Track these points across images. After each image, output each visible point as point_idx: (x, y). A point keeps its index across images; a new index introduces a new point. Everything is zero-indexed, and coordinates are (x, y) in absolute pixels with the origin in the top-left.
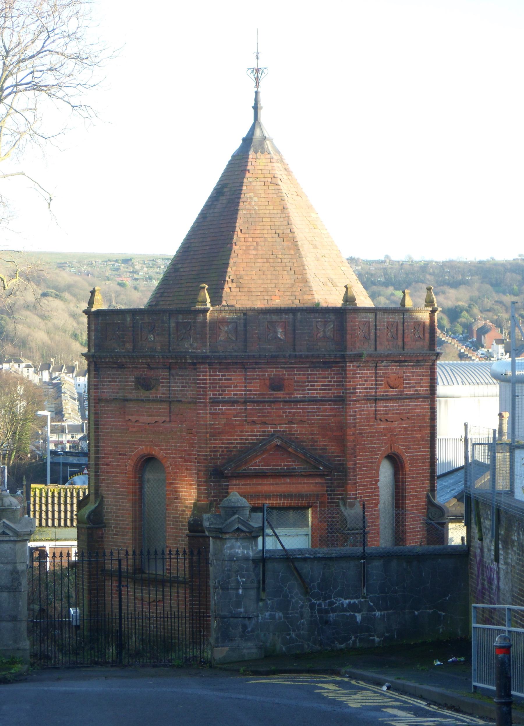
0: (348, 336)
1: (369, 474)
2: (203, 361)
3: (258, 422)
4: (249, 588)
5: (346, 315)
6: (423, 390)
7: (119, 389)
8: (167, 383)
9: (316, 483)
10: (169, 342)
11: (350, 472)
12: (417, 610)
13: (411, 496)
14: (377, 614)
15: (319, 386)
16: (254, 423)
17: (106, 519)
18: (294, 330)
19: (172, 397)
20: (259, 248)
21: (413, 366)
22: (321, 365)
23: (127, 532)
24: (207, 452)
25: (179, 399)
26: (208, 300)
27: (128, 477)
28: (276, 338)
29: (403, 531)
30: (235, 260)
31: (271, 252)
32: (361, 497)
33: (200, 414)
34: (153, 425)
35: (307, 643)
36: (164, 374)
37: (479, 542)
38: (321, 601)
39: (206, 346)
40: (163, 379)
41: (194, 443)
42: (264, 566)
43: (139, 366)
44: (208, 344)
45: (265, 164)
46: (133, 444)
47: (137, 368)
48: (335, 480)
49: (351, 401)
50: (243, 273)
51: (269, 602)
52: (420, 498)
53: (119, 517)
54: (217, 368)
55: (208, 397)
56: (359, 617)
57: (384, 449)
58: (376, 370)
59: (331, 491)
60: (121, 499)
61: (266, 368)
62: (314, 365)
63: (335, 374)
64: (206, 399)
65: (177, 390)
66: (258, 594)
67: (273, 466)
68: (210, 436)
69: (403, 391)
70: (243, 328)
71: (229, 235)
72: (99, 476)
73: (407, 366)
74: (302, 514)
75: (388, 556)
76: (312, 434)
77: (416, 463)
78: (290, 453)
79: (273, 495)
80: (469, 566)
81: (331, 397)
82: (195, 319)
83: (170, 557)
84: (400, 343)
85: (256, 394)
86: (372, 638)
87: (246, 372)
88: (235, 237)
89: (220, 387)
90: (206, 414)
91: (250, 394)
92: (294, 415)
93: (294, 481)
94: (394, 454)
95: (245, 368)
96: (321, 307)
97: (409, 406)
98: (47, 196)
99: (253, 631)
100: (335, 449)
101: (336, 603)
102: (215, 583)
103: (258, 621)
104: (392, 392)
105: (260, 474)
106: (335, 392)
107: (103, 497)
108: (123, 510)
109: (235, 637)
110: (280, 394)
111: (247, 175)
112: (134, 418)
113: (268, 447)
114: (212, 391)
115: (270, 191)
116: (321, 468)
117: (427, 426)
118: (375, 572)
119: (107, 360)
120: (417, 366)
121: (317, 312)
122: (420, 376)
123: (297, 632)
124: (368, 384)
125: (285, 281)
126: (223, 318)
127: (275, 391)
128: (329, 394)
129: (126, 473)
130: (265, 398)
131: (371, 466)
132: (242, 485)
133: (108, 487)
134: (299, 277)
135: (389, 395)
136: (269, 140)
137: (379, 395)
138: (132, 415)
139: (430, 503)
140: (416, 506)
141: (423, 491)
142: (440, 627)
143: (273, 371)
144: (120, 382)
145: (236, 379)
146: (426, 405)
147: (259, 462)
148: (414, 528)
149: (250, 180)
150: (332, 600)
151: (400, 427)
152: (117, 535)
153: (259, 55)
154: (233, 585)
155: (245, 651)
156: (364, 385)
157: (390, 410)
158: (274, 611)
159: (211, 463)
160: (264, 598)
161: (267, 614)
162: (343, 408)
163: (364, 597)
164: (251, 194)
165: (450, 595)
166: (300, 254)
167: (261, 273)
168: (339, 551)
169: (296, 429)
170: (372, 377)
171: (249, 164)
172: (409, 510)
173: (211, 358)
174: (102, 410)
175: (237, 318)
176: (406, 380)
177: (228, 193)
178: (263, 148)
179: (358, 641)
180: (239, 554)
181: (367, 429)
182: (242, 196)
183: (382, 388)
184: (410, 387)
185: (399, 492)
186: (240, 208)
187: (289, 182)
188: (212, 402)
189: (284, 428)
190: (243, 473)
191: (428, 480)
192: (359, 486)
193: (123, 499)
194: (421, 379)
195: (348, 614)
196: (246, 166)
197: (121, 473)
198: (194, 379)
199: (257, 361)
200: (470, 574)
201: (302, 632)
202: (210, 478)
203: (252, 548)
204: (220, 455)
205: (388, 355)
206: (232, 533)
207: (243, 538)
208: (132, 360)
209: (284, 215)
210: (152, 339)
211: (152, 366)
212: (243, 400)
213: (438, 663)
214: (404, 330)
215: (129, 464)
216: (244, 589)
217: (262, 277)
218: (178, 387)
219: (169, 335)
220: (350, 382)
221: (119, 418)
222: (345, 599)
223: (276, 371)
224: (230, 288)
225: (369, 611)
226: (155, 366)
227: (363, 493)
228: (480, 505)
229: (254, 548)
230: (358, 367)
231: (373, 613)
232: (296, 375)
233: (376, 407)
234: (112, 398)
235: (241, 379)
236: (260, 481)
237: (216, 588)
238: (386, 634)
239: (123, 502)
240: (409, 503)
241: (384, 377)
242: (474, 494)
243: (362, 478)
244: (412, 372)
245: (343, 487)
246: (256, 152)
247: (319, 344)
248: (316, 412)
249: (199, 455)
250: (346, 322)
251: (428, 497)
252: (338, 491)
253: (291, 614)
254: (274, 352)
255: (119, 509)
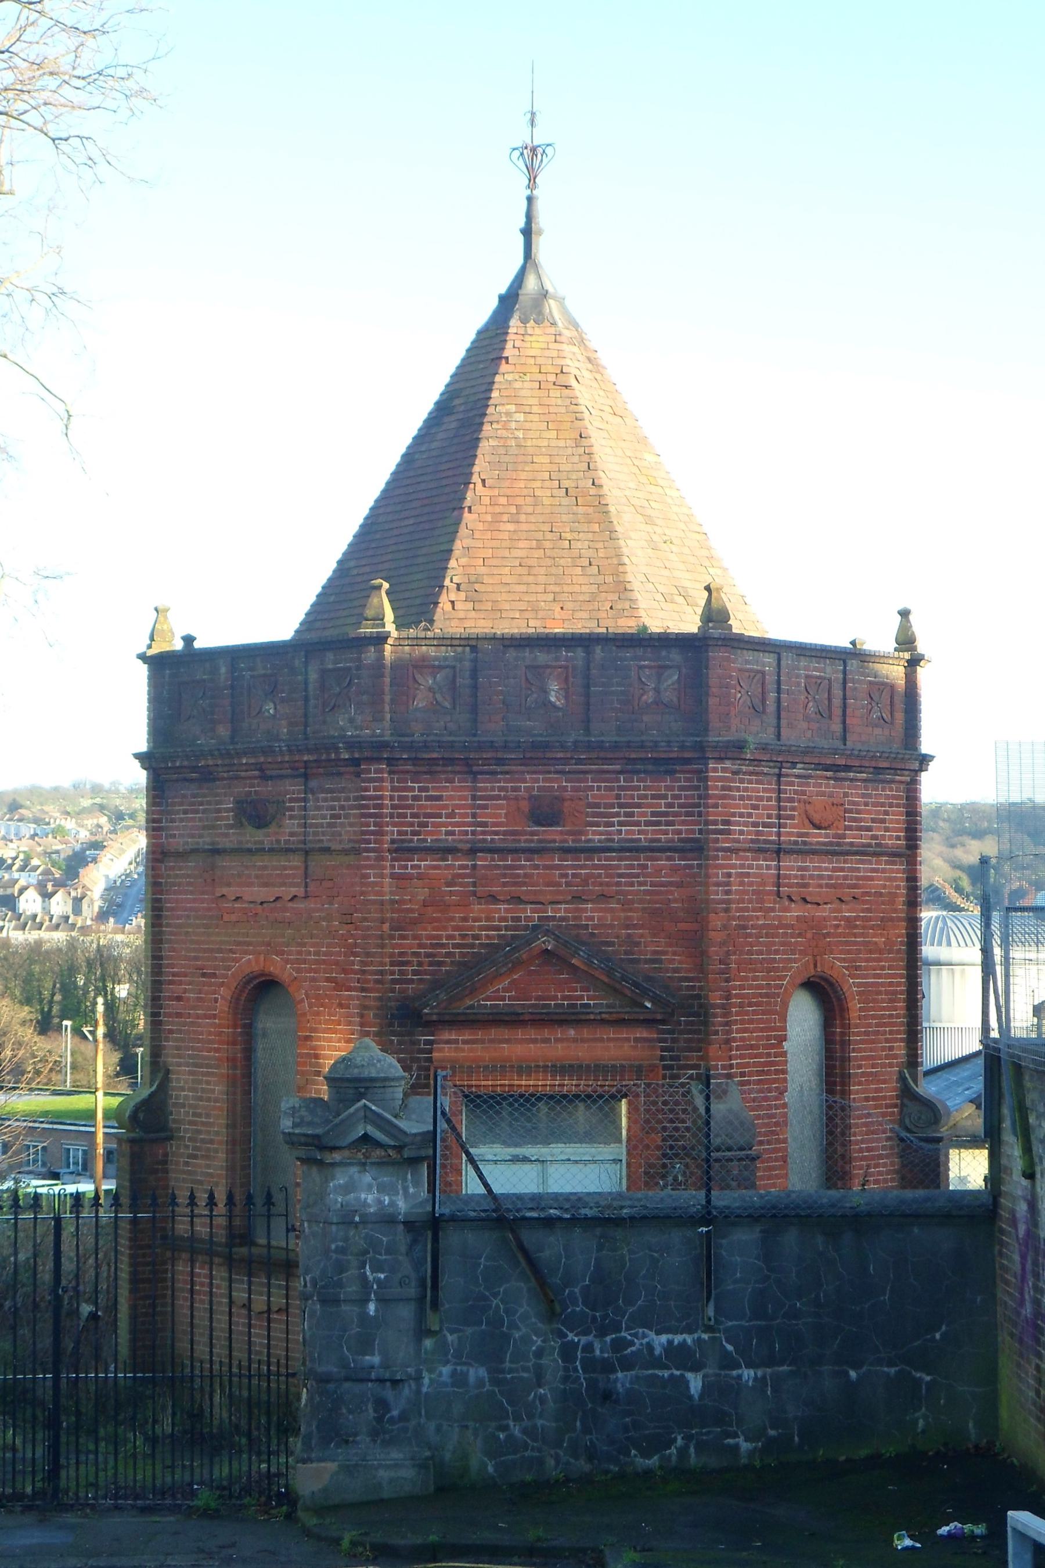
0: (712, 701)
1: (761, 1021)
2: (375, 755)
3: (502, 898)
4: (395, 1300)
5: (707, 651)
6: (890, 838)
7: (204, 828)
8: (301, 808)
9: (636, 1040)
10: (306, 716)
11: (715, 1016)
12: (856, 1366)
13: (863, 1074)
14: (745, 1377)
15: (644, 814)
16: (493, 898)
17: (175, 1121)
18: (588, 686)
19: (310, 841)
20: (523, 518)
21: (864, 781)
22: (650, 767)
23: (216, 1151)
24: (382, 964)
25: (326, 845)
26: (389, 615)
27: (220, 1026)
28: (547, 704)
29: (843, 1156)
30: (467, 542)
31: (547, 527)
32: (743, 1074)
33: (368, 876)
34: (272, 905)
35: (552, 1452)
36: (293, 788)
37: (1025, 1182)
38: (590, 1338)
39: (382, 720)
40: (291, 800)
41: (356, 945)
42: (435, 1240)
43: (243, 774)
44: (388, 716)
45: (544, 346)
46: (231, 951)
47: (237, 778)
48: (681, 1032)
49: (718, 850)
50: (483, 570)
51: (450, 1338)
52: (884, 1082)
53: (199, 1115)
54: (408, 772)
55: (388, 838)
56: (695, 1383)
57: (798, 966)
58: (779, 783)
59: (672, 1058)
60: (203, 1074)
61: (523, 772)
62: (632, 767)
63: (681, 788)
64: (380, 842)
65: (322, 825)
66: (420, 1317)
67: (538, 998)
68: (392, 929)
69: (844, 836)
70: (468, 682)
71: (456, 492)
72: (160, 1023)
73: (851, 780)
74: (606, 1115)
75: (774, 1216)
76: (627, 927)
77: (875, 1001)
78: (575, 968)
79: (538, 1066)
80: (997, 1248)
81: (672, 840)
82: (359, 659)
83: (192, 1211)
84: (837, 727)
85: (496, 833)
86: (731, 1441)
87: (475, 780)
88: (469, 495)
89: (413, 816)
90: (382, 876)
91: (484, 833)
92: (585, 882)
93: (586, 1033)
94: (821, 978)
95: (471, 772)
96: (652, 633)
97: (858, 870)
98: (60, 408)
99: (404, 1417)
100: (680, 962)
101: (632, 1344)
102: (305, 1285)
103: (418, 1392)
104: (819, 837)
105: (507, 1018)
106: (681, 829)
107: (168, 1072)
108: (209, 1100)
109: (356, 1435)
110: (553, 834)
111: (504, 367)
112: (231, 892)
113: (523, 954)
114: (395, 825)
115: (553, 401)
116: (649, 1005)
117: (899, 919)
118: (739, 1259)
119: (178, 764)
120: (875, 781)
121: (640, 646)
122: (883, 805)
123: (526, 1423)
124: (760, 815)
125: (577, 588)
126: (424, 658)
127: (544, 826)
128: (668, 835)
129: (214, 1016)
130: (519, 841)
131: (768, 1004)
132: (465, 1042)
133: (178, 1048)
134: (609, 579)
135: (811, 844)
136: (554, 298)
137: (785, 842)
138: (229, 885)
139: (907, 1093)
140: (874, 1099)
141: (891, 1065)
142: (917, 1415)
143: (537, 781)
144: (204, 811)
145: (451, 798)
146: (898, 871)
147: (505, 990)
148: (869, 1149)
149: (507, 377)
150: (623, 1334)
151: (836, 919)
152: (195, 1157)
153: (538, 119)
154: (352, 1289)
155: (381, 1473)
156: (750, 815)
157: (811, 877)
158: (465, 1364)
159: (393, 991)
160: (436, 1328)
161: (446, 1370)
162: (699, 866)
163: (709, 1329)
164: (508, 407)
165: (944, 1328)
166: (612, 531)
167: (524, 571)
168: (640, 1200)
169: (591, 913)
170: (769, 799)
171: (509, 345)
172: (858, 1109)
173: (393, 747)
174: (169, 877)
175: (455, 658)
176: (850, 811)
177: (462, 408)
178: (540, 313)
179: (692, 1450)
180: (369, 1206)
181: (757, 918)
182: (490, 410)
183: (793, 826)
184: (860, 829)
185: (834, 1067)
186: (483, 434)
187: (597, 386)
188: (396, 850)
189: (562, 911)
190: (466, 1014)
191: (901, 1040)
192: (738, 1048)
193: (208, 1074)
194: (886, 813)
195: (666, 1374)
196: (503, 349)
197: (206, 1017)
198: (356, 799)
199: (500, 755)
200: (998, 1271)
201: (540, 1422)
202: (391, 1025)
203: (405, 1190)
204: (415, 973)
205: (808, 751)
206: (349, 1147)
207: (380, 1164)
208: (227, 761)
209: (581, 450)
210: (271, 711)
211: (268, 773)
212: (469, 845)
213: (908, 1542)
214: (845, 698)
215: (223, 997)
216: (381, 1300)
217: (526, 579)
218: (324, 817)
219: (306, 699)
220: (716, 806)
221: (203, 893)
222: (658, 1333)
223: (545, 780)
224: (453, 602)
225: (723, 1367)
226: (275, 773)
227: (747, 1065)
228: (1027, 1077)
229: (411, 1190)
230: (735, 773)
231: (735, 1373)
232: (592, 788)
233: (779, 868)
234: (188, 848)
235: (465, 798)
236: (505, 1033)
237: (306, 1299)
238: (772, 1433)
239: (208, 1083)
240: (857, 1092)
241: (799, 801)
242: (1009, 1046)
243: (745, 1030)
244: (863, 796)
245: (699, 1050)
246: (524, 321)
247: (645, 718)
248: (637, 876)
249: (364, 972)
250: (707, 668)
251: (902, 1079)
252: (687, 1058)
253: (511, 1371)
254: (541, 735)
255: (201, 1099)
